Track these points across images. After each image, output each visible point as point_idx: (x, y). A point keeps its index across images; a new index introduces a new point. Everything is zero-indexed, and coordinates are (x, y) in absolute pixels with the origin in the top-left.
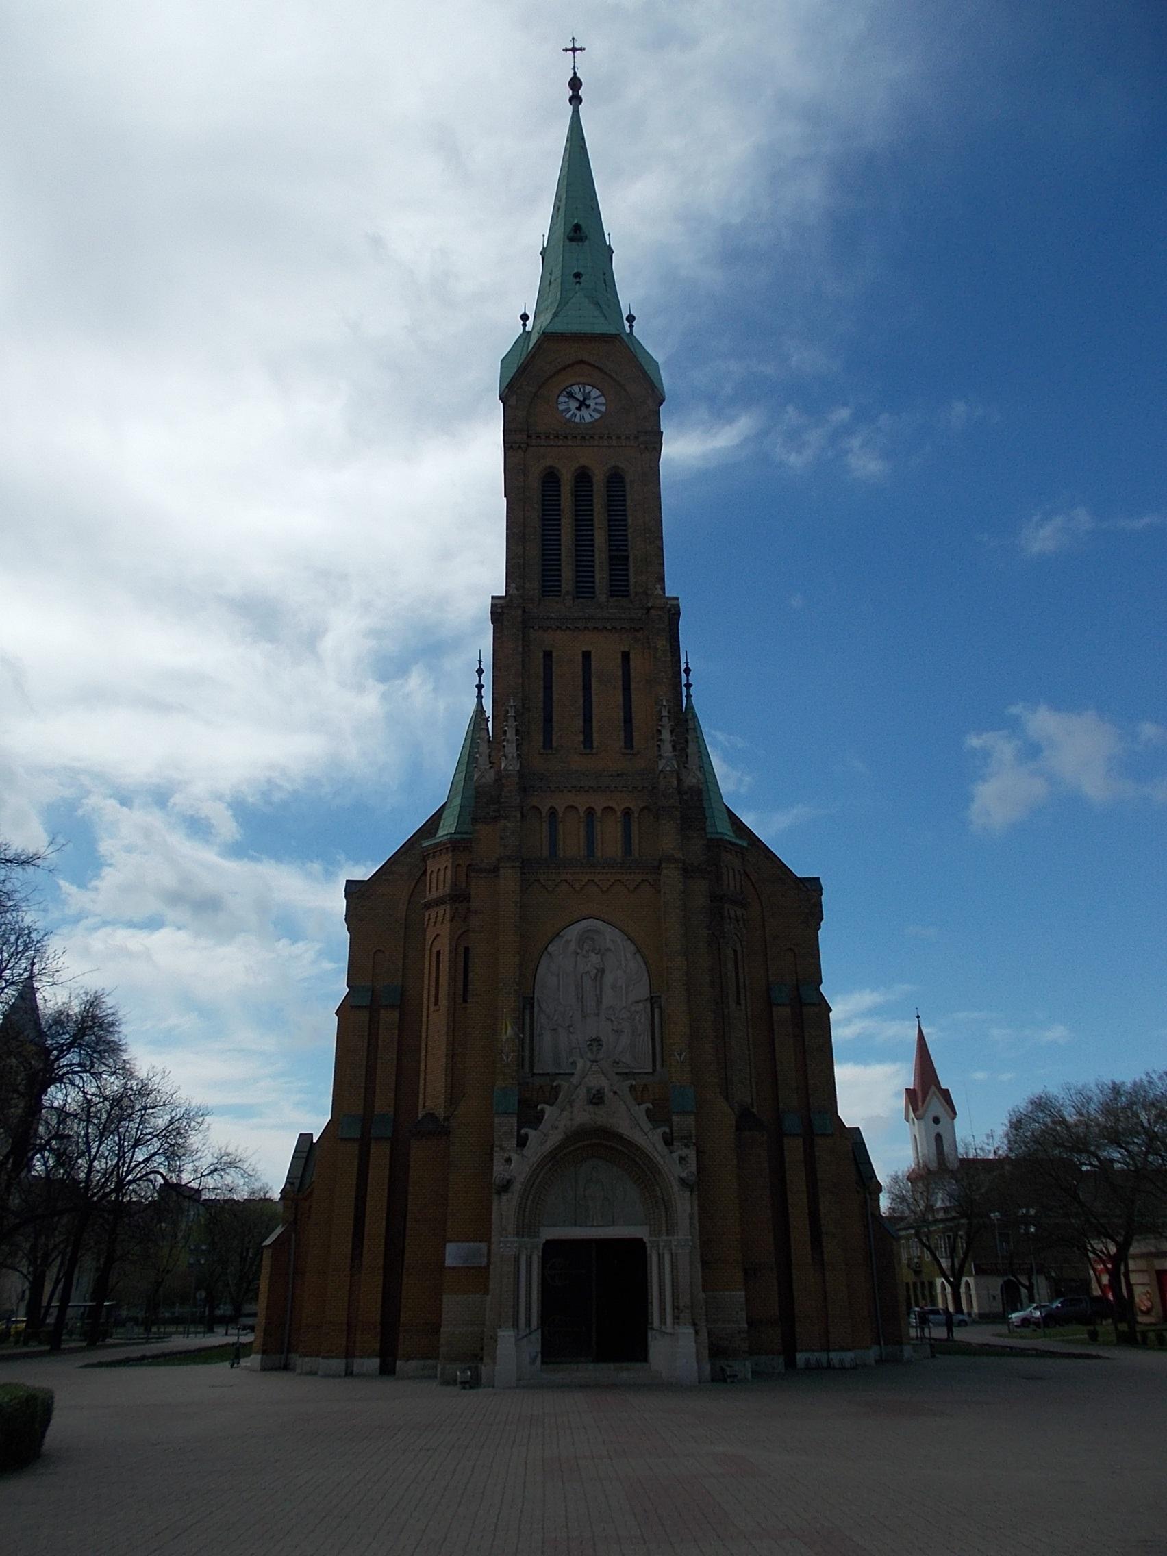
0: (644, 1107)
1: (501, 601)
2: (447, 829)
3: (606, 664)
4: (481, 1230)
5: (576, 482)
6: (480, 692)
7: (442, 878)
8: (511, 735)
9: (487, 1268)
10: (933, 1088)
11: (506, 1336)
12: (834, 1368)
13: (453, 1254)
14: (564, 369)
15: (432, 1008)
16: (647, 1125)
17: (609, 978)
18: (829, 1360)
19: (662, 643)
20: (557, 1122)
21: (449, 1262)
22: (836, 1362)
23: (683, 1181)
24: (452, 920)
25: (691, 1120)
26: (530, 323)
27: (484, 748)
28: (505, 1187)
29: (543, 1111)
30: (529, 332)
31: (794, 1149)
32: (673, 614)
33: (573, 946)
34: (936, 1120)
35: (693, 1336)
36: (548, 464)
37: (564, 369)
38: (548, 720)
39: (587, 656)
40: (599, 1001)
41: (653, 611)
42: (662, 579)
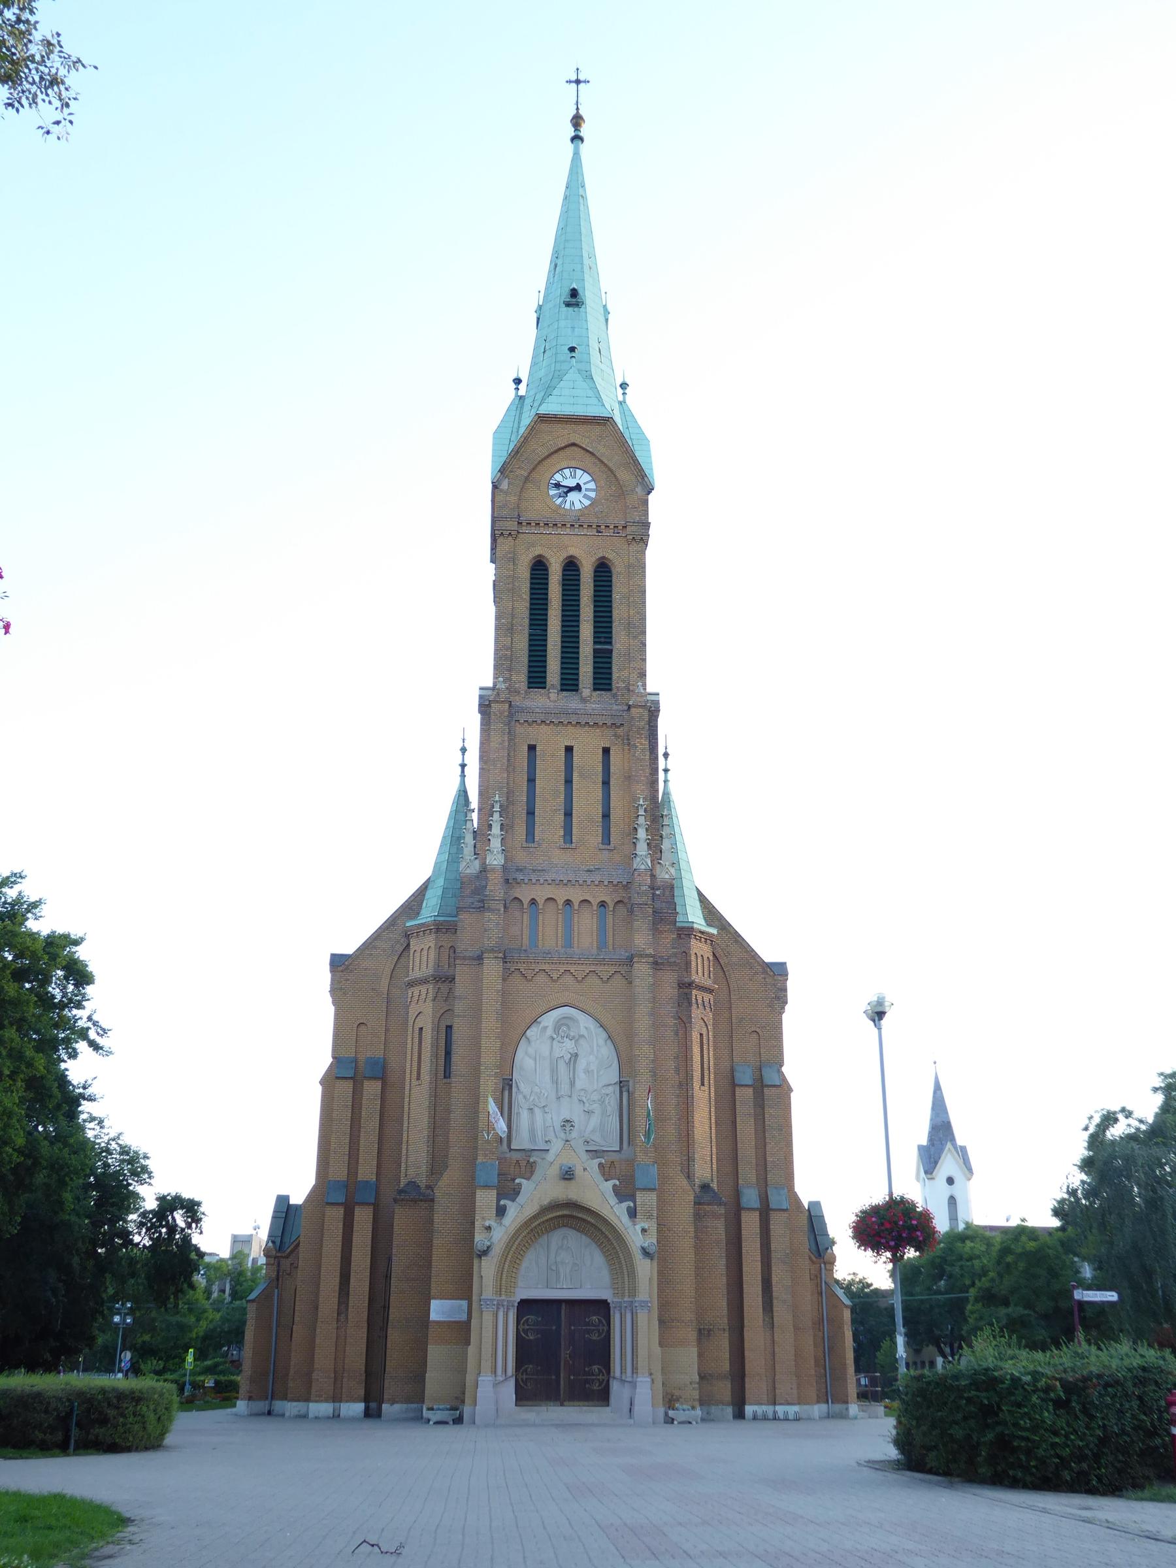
0: (610, 1183)
1: (490, 692)
2: (429, 912)
3: (588, 759)
4: (464, 1288)
5: (564, 570)
6: (463, 771)
7: (425, 959)
8: (496, 830)
9: (468, 1323)
10: (949, 1145)
11: (486, 1380)
12: (779, 1419)
13: (438, 1310)
14: (556, 452)
15: (414, 1082)
16: (613, 1200)
17: (582, 1063)
18: (775, 1412)
19: (642, 743)
20: (535, 1193)
21: (433, 1316)
22: (781, 1415)
23: (646, 1253)
24: (434, 1000)
25: (653, 1196)
26: (523, 388)
27: (469, 839)
28: (485, 1252)
29: (520, 1185)
30: (521, 397)
31: (750, 1223)
32: (653, 711)
33: (549, 1032)
34: (950, 1181)
35: (649, 1385)
36: (537, 553)
37: (556, 452)
38: (531, 813)
39: (569, 749)
40: (572, 1084)
41: (633, 710)
42: (643, 675)
